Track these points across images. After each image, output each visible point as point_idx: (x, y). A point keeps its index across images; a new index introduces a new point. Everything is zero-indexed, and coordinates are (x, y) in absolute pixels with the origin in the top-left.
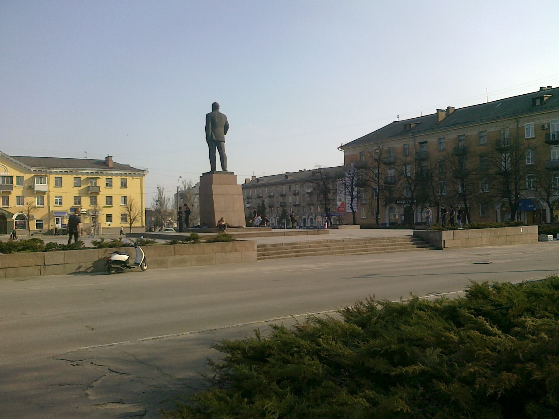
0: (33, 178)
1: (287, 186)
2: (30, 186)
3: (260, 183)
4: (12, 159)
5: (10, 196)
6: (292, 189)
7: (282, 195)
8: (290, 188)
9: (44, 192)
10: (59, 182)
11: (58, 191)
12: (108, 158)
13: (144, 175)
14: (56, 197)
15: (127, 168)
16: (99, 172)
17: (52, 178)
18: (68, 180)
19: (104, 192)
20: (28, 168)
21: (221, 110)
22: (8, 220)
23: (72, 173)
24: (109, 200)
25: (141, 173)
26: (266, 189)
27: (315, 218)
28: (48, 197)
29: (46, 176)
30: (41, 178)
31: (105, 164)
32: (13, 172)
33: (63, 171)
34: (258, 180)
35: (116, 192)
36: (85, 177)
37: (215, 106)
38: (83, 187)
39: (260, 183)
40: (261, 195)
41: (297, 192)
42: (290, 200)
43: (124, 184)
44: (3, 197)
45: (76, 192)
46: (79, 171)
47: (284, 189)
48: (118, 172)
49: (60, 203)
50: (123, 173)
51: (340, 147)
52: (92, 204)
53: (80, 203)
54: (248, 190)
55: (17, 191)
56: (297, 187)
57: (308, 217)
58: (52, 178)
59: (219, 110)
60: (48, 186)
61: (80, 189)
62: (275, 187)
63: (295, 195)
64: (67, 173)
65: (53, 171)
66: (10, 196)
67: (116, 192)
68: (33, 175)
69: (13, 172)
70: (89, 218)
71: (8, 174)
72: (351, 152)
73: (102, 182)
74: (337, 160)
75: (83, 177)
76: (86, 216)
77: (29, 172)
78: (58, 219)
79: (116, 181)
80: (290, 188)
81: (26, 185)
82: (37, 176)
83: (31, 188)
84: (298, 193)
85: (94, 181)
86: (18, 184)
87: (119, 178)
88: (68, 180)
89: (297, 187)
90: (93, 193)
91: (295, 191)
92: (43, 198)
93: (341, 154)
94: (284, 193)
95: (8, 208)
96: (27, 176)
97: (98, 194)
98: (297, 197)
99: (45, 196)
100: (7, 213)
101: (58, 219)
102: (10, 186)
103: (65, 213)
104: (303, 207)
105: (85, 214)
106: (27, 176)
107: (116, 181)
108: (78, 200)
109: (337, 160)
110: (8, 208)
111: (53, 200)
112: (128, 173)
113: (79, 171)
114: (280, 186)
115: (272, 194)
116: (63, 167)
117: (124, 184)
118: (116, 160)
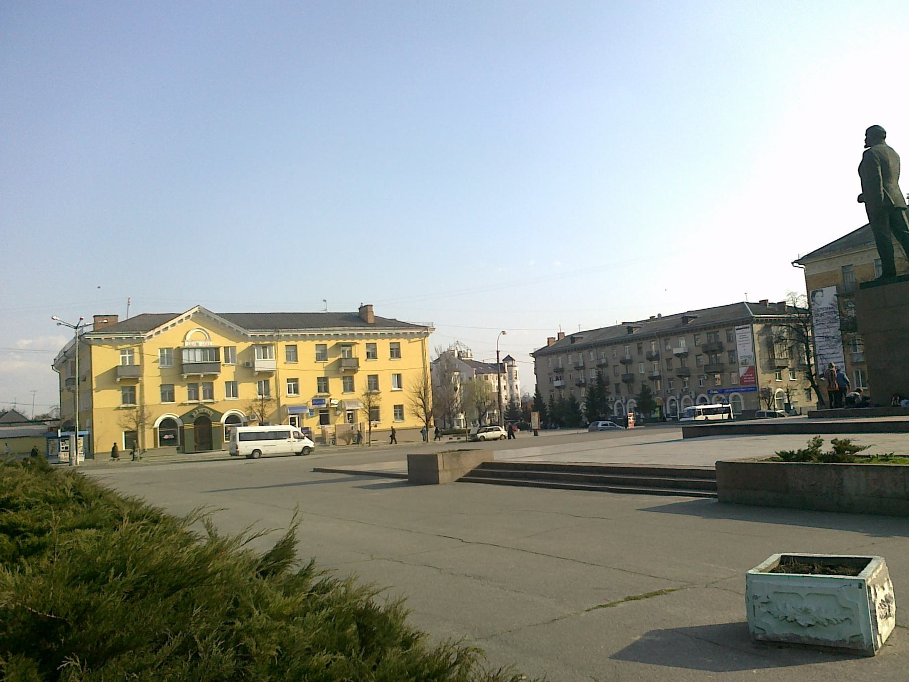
0: (251, 349)
1: (634, 345)
2: (248, 364)
3: (577, 343)
4: (218, 318)
5: (214, 382)
6: (645, 350)
7: (624, 362)
8: (639, 348)
9: (269, 374)
10: (292, 355)
11: (397, 365)
12: (365, 310)
13: (427, 335)
14: (288, 380)
15: (393, 324)
16: (356, 333)
17: (281, 346)
18: (307, 349)
19: (366, 368)
20: (242, 331)
21: (889, 141)
22: (214, 425)
23: (312, 337)
24: (373, 381)
25: (422, 331)
26: (591, 354)
27: (625, 404)
28: (277, 380)
29: (271, 345)
30: (264, 347)
31: (361, 318)
32: (218, 340)
33: (299, 334)
34: (572, 338)
35: (383, 366)
36: (333, 342)
37: (875, 135)
38: (331, 360)
39: (577, 343)
40: (581, 365)
41: (654, 354)
42: (641, 369)
43: (395, 353)
44: (189, 384)
45: (319, 369)
46: (324, 334)
47: (628, 351)
48: (386, 332)
49: (296, 391)
50: (394, 332)
51: (796, 262)
52: (345, 390)
53: (327, 390)
54: (554, 357)
55: (227, 373)
56: (653, 347)
57: (681, 397)
58: (281, 346)
59: (886, 140)
60: (273, 362)
61: (325, 365)
62: (609, 348)
63: (651, 359)
64: (304, 338)
65: (283, 334)
66: (214, 382)
67: (383, 366)
68: (250, 344)
69: (218, 340)
70: (342, 415)
71: (212, 344)
72: (821, 268)
73: (360, 351)
74: (789, 287)
75: (331, 344)
76: (338, 412)
77: (245, 338)
78: (293, 420)
79: (383, 347)
80: (639, 348)
81: (241, 362)
82: (257, 345)
83: (248, 366)
84: (657, 355)
85: (348, 349)
86: (227, 360)
87: (363, 342)
88: (307, 349)
89: (653, 347)
90: (346, 370)
91: (650, 353)
92: (267, 382)
93: (800, 273)
94: (628, 357)
95: (213, 403)
96: (241, 346)
97: (355, 371)
98: (656, 363)
99: (272, 380)
100: (211, 413)
101: (293, 420)
102: (216, 366)
103: (305, 408)
104: (669, 380)
105: (337, 409)
106: (241, 346)
107: (383, 347)
108: (323, 384)
109: (789, 287)
110: (213, 403)
111: (284, 386)
112: (401, 332)
113: (324, 334)
114: (620, 347)
115: (604, 361)
116: (297, 327)
117: (395, 353)
118: (379, 311)
